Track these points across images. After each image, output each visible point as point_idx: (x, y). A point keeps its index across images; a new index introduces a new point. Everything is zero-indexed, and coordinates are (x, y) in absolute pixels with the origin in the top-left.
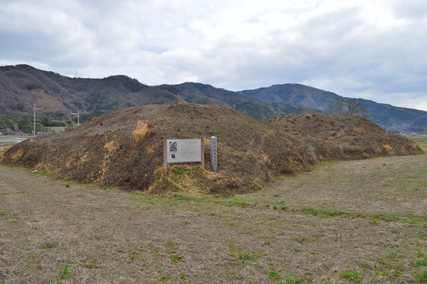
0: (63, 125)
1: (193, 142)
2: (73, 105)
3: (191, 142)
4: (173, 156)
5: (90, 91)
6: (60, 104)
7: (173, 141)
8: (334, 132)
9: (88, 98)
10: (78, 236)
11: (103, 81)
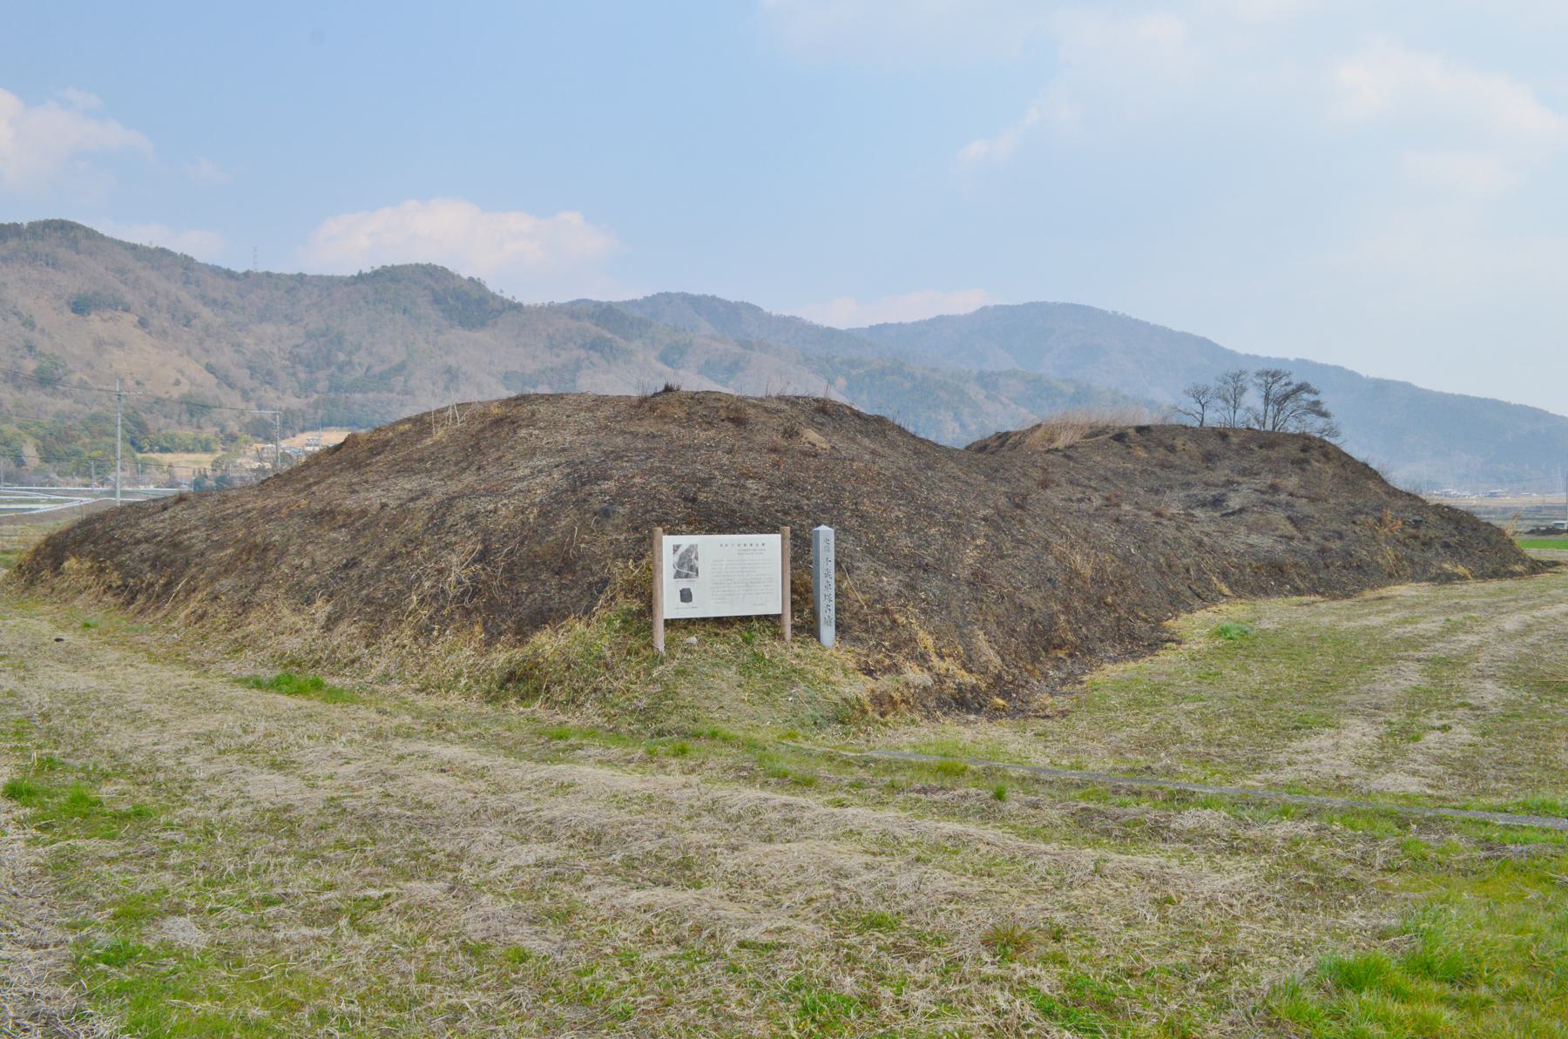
0: (206, 448)
2: (242, 376)
4: (686, 596)
5: (305, 322)
6: (195, 370)
7: (685, 541)
8: (1214, 492)
9: (297, 346)
10: (741, 886)
11: (355, 284)
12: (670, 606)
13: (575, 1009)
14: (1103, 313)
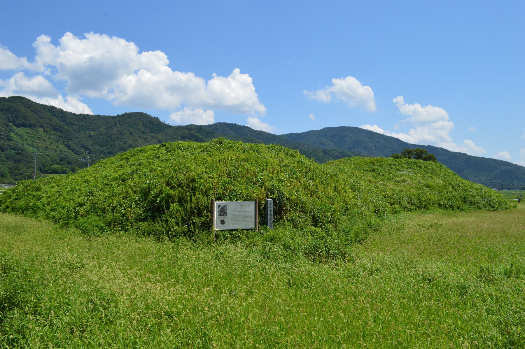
1: (246, 206)
3: (244, 206)
4: (223, 222)
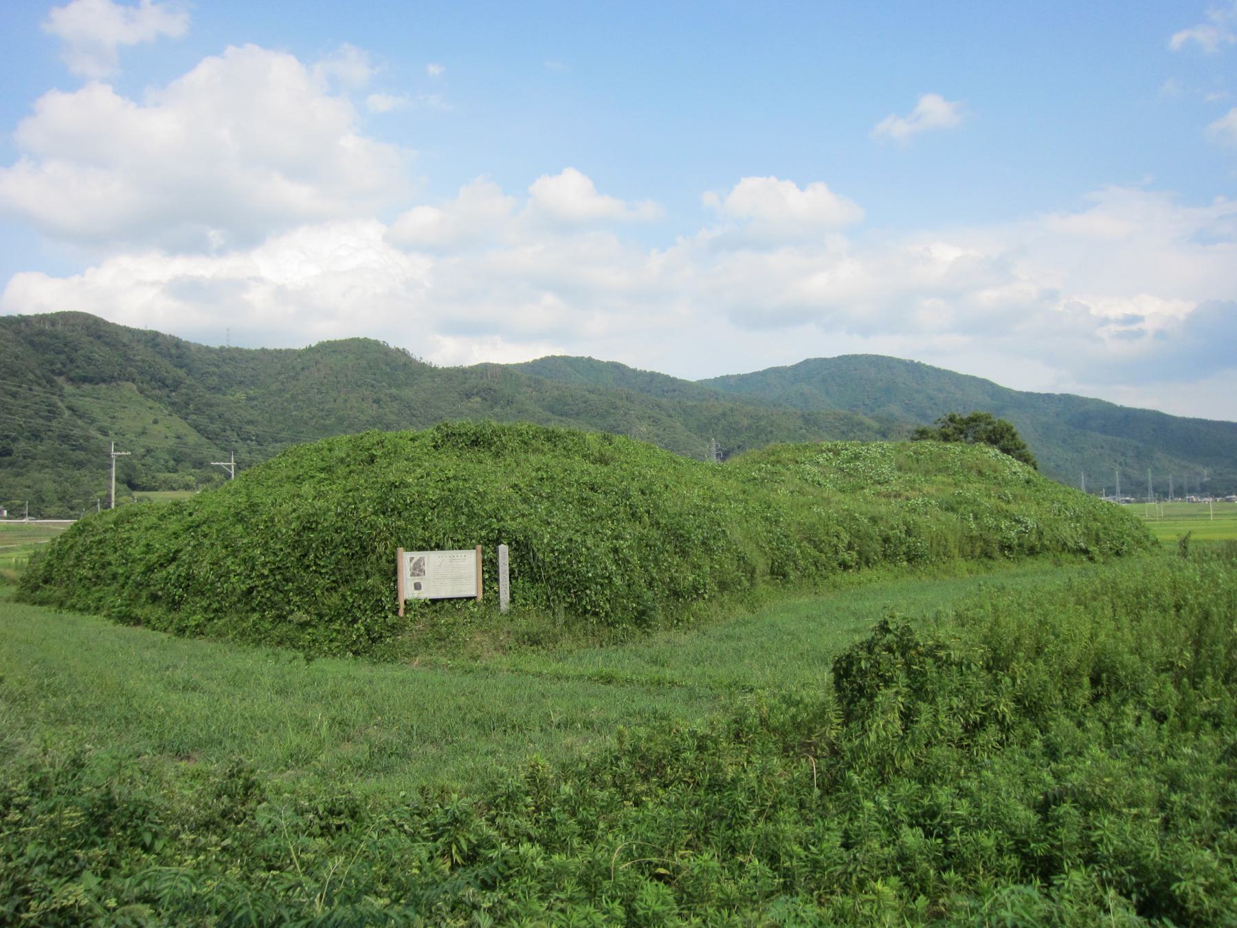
4: (418, 586)
7: (417, 555)
12: (407, 591)
13: (1016, 709)
14: (801, 363)
